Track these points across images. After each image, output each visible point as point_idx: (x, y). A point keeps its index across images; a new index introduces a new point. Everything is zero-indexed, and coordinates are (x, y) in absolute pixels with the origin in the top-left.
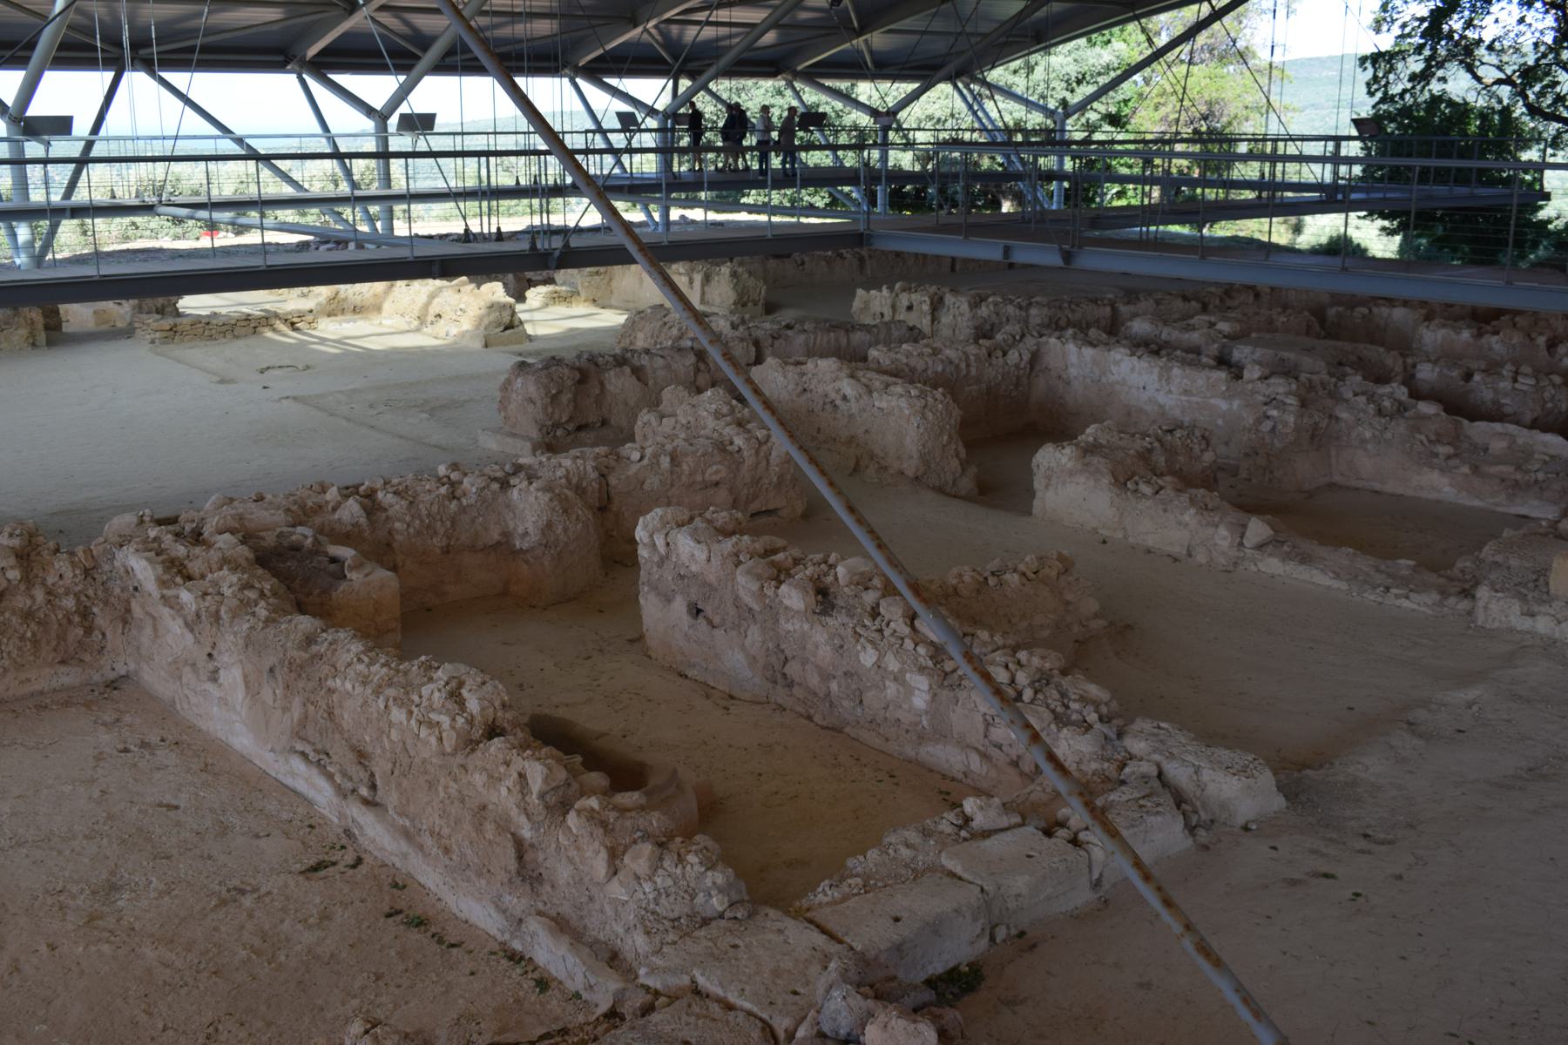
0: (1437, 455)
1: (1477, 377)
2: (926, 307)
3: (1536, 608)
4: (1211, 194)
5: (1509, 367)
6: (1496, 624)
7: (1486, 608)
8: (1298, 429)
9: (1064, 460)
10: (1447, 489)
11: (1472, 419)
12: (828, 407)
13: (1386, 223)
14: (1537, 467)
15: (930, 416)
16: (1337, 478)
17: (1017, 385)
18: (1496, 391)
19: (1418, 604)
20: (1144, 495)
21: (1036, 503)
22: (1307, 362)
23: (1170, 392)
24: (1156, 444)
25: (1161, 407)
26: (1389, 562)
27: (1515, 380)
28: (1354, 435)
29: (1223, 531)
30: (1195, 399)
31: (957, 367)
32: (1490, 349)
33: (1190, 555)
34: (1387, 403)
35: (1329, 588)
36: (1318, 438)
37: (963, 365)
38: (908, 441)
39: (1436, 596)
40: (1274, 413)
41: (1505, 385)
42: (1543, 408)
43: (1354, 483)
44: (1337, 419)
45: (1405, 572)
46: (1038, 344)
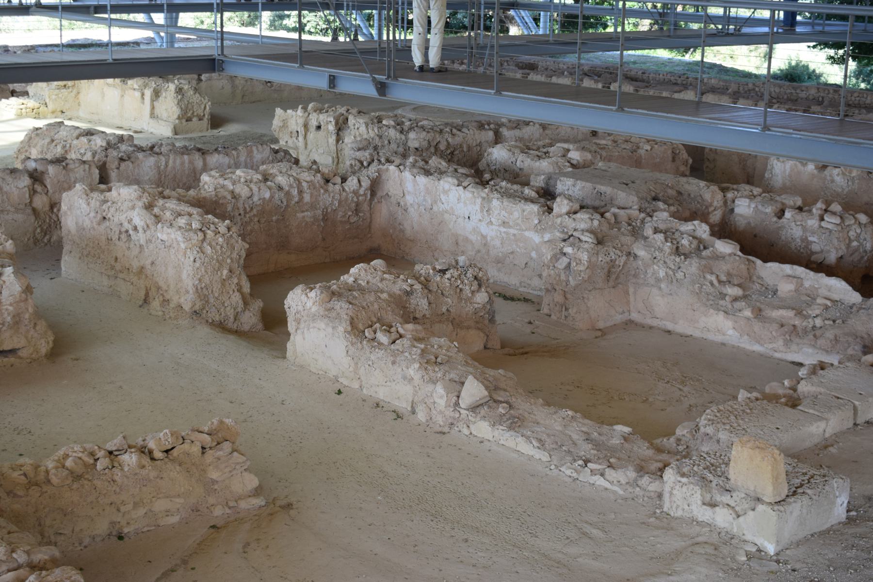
0: (723, 296)
1: (788, 214)
2: (331, 127)
3: (718, 498)
4: (695, 26)
5: (820, 205)
6: (679, 513)
7: (671, 494)
8: (591, 266)
9: (309, 304)
10: (731, 332)
11: (766, 259)
12: (123, 236)
13: (832, 52)
14: (818, 312)
15: (208, 250)
16: (635, 316)
17: (357, 211)
18: (804, 229)
19: (613, 482)
20: (380, 344)
21: (289, 345)
22: (622, 196)
23: (491, 223)
24: (418, 287)
25: (484, 237)
26: (605, 429)
27: (822, 219)
28: (650, 271)
29: (440, 390)
30: (512, 231)
31: (288, 193)
32: (833, 181)
33: (414, 412)
34: (685, 242)
35: (530, 458)
36: (614, 277)
37: (295, 192)
38: (184, 276)
39: (632, 474)
40: (569, 250)
41: (813, 223)
42: (848, 246)
43: (649, 321)
44: (636, 256)
45: (616, 441)
46: (378, 171)
